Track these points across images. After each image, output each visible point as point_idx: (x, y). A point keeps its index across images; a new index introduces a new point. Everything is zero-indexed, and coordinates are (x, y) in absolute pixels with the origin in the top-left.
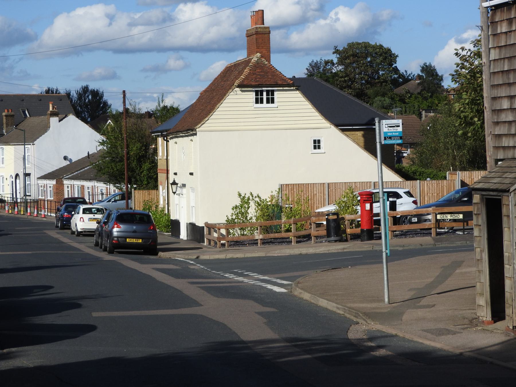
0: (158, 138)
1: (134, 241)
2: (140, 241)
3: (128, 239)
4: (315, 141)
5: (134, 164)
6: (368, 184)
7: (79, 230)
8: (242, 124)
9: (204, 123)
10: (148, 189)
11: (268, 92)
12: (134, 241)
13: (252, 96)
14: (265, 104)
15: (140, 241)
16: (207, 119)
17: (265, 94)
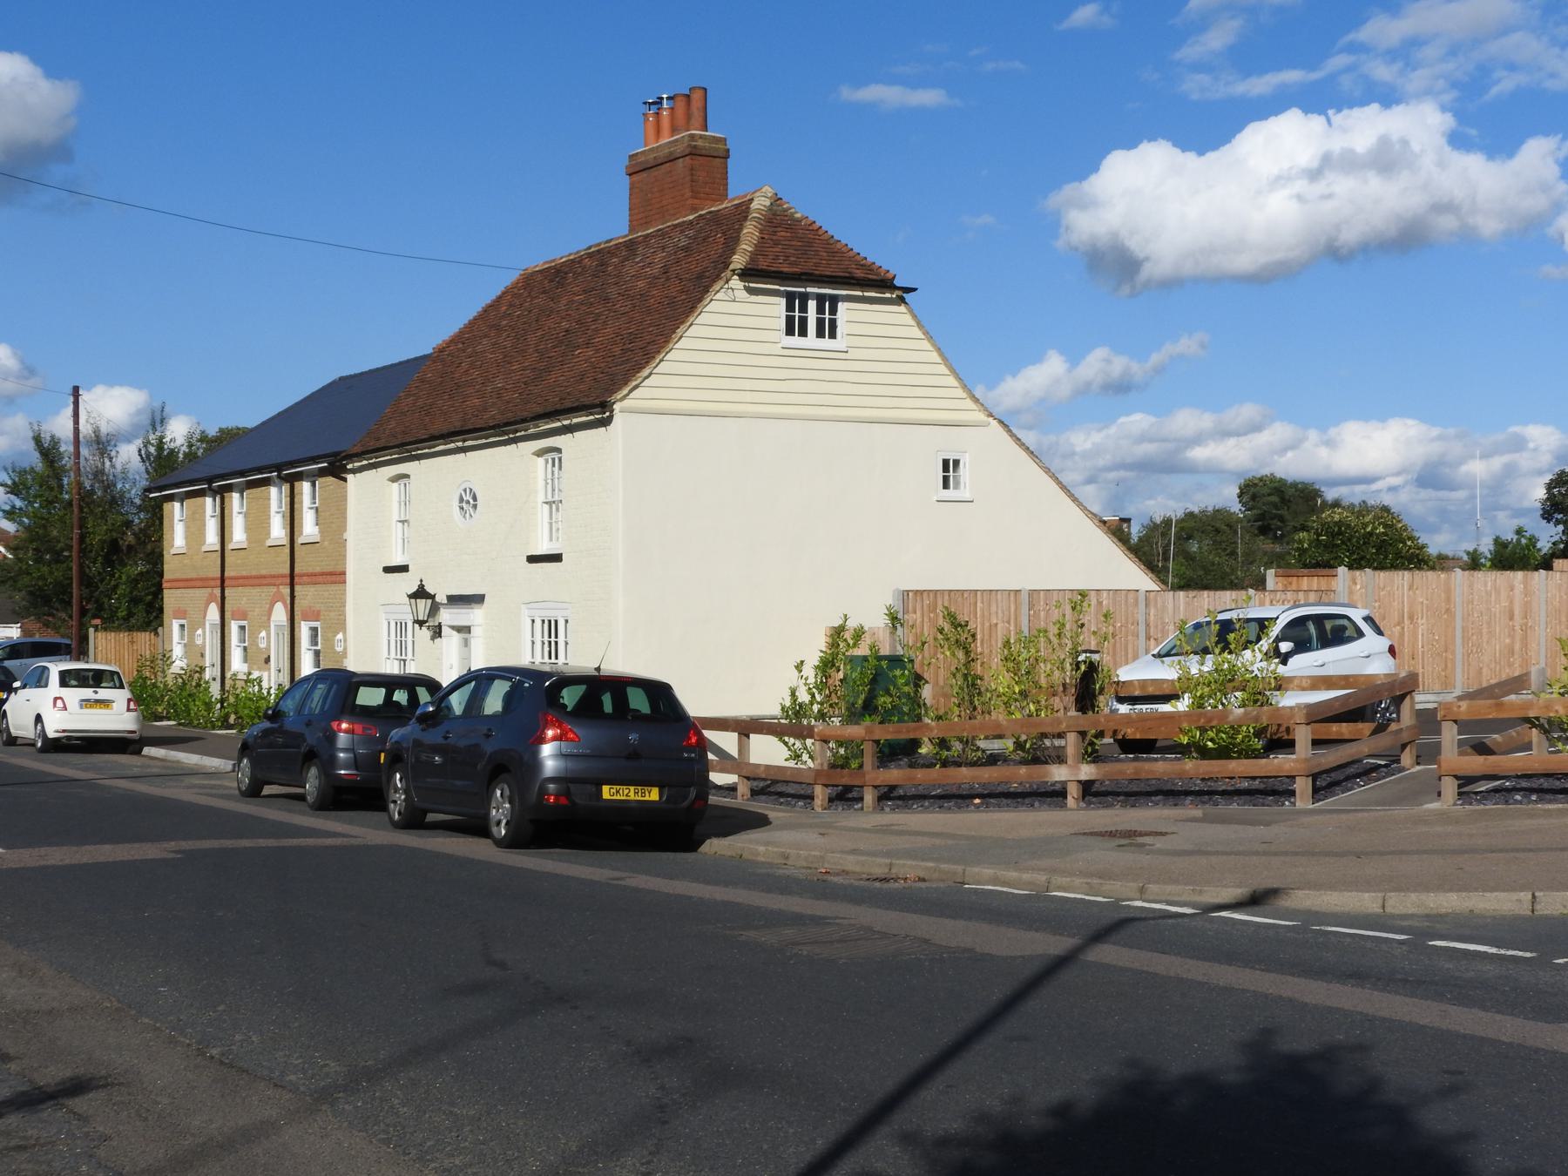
0: (166, 506)
1: (630, 794)
2: (654, 795)
3: (605, 788)
4: (946, 463)
5: (94, 569)
6: (1131, 595)
7: (51, 734)
8: (749, 397)
9: (637, 387)
10: (130, 629)
11: (821, 299)
12: (630, 794)
13: (777, 308)
14: (812, 339)
15: (654, 795)
16: (646, 372)
17: (812, 305)
